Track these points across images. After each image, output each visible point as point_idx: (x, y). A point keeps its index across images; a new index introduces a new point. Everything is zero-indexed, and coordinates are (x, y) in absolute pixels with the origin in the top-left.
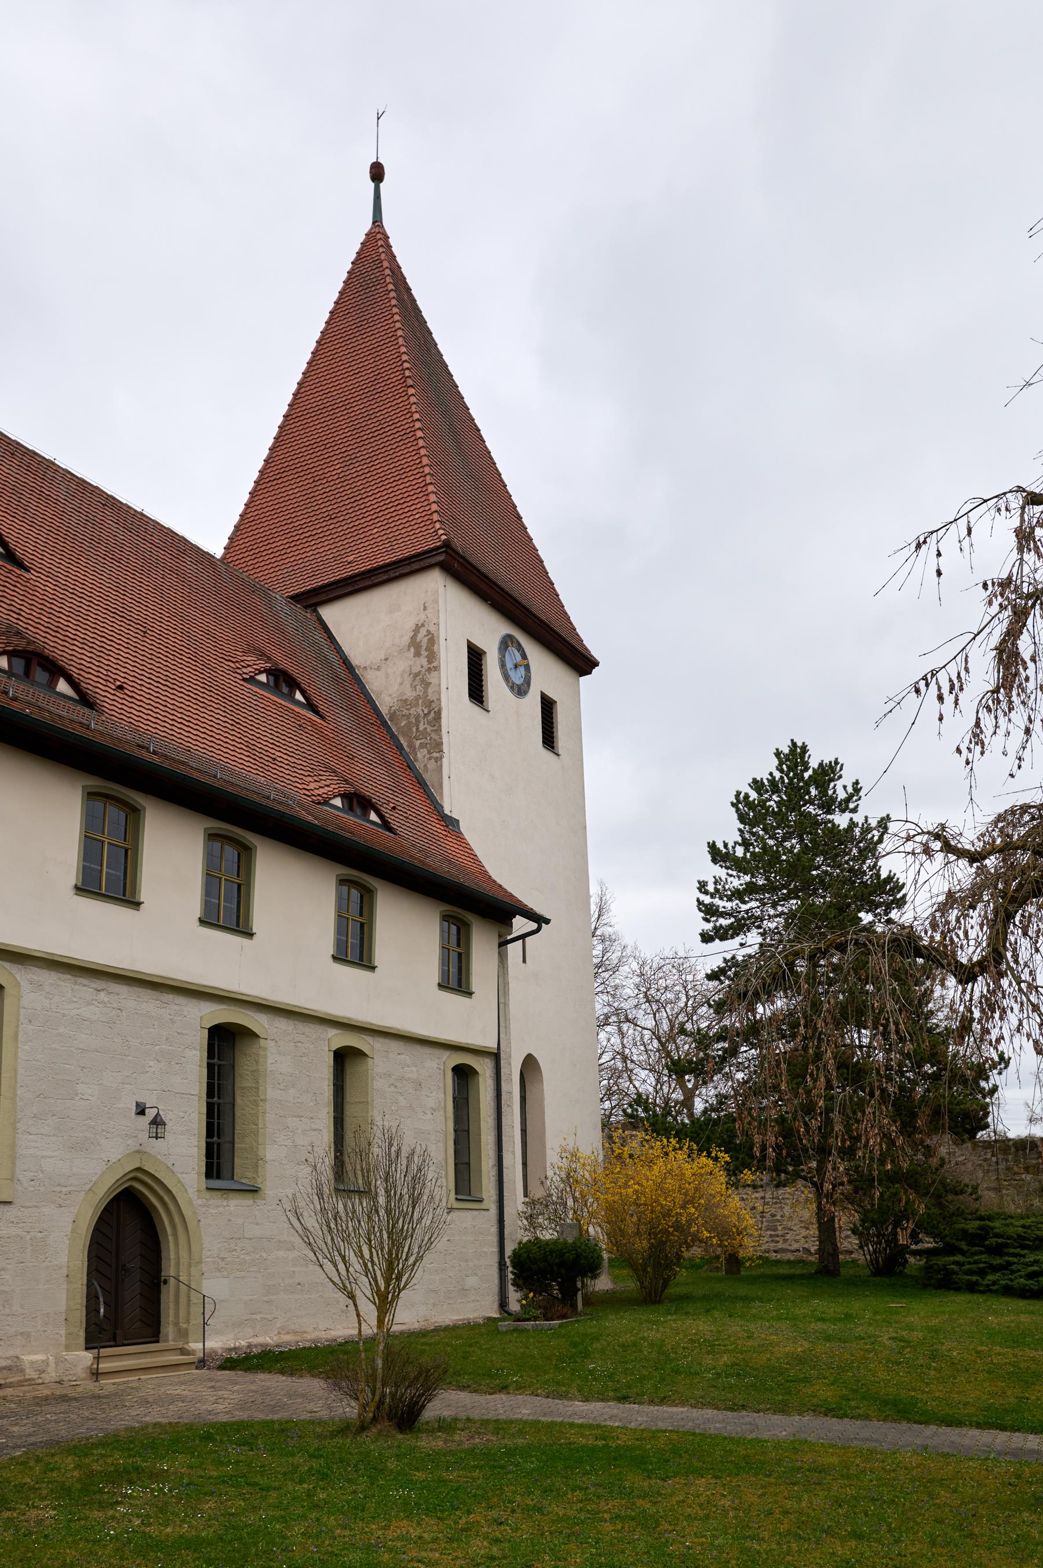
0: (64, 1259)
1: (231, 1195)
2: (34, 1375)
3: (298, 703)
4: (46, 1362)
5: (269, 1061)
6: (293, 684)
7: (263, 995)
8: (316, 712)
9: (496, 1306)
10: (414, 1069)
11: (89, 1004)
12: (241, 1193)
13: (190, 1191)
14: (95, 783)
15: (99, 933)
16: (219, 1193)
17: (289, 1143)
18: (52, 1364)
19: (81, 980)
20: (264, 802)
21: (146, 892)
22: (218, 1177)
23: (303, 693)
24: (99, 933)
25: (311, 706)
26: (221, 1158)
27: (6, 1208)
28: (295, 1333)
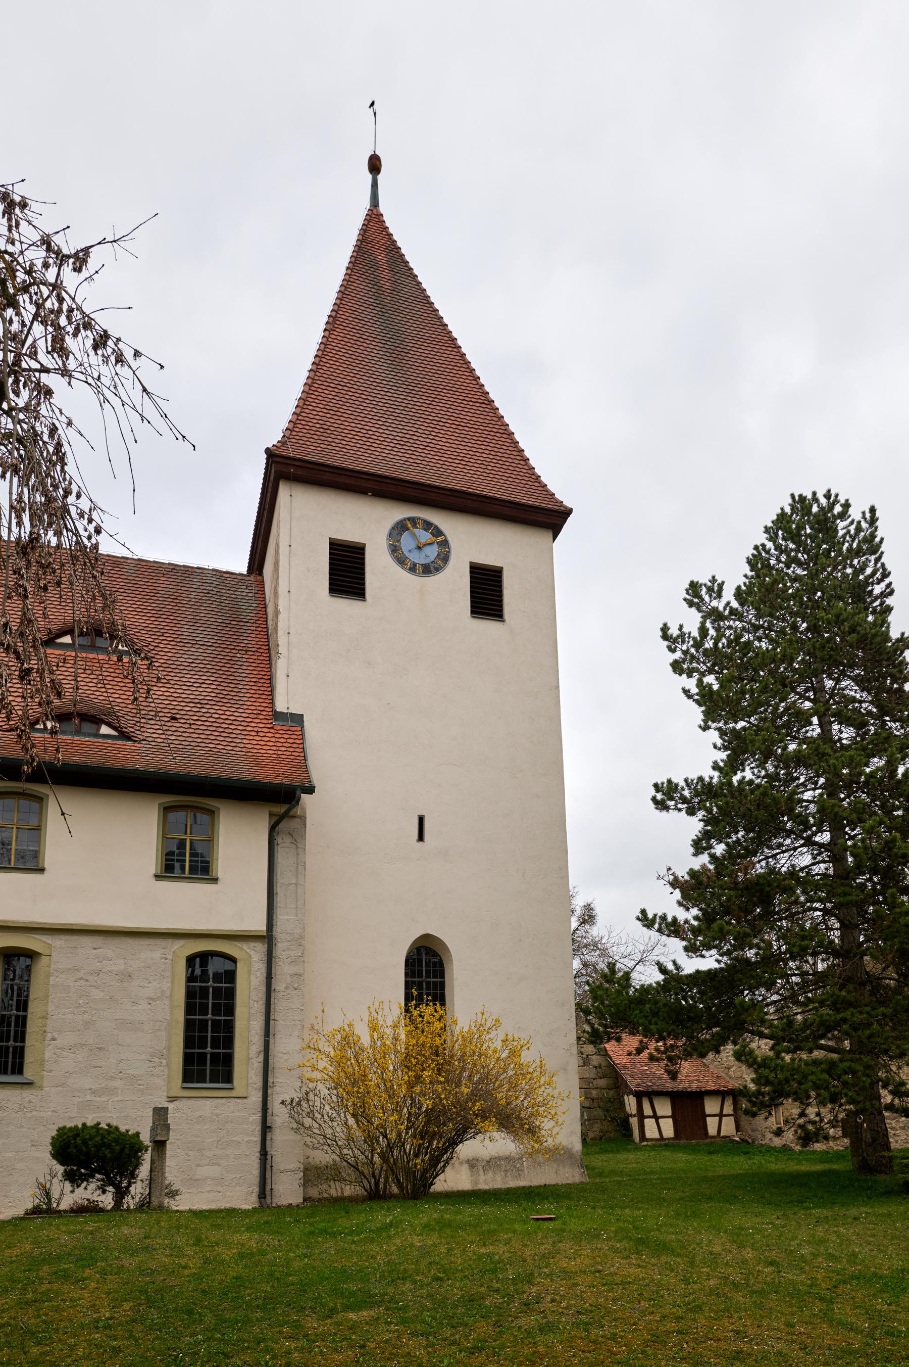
7: (196, 928)
10: (122, 961)
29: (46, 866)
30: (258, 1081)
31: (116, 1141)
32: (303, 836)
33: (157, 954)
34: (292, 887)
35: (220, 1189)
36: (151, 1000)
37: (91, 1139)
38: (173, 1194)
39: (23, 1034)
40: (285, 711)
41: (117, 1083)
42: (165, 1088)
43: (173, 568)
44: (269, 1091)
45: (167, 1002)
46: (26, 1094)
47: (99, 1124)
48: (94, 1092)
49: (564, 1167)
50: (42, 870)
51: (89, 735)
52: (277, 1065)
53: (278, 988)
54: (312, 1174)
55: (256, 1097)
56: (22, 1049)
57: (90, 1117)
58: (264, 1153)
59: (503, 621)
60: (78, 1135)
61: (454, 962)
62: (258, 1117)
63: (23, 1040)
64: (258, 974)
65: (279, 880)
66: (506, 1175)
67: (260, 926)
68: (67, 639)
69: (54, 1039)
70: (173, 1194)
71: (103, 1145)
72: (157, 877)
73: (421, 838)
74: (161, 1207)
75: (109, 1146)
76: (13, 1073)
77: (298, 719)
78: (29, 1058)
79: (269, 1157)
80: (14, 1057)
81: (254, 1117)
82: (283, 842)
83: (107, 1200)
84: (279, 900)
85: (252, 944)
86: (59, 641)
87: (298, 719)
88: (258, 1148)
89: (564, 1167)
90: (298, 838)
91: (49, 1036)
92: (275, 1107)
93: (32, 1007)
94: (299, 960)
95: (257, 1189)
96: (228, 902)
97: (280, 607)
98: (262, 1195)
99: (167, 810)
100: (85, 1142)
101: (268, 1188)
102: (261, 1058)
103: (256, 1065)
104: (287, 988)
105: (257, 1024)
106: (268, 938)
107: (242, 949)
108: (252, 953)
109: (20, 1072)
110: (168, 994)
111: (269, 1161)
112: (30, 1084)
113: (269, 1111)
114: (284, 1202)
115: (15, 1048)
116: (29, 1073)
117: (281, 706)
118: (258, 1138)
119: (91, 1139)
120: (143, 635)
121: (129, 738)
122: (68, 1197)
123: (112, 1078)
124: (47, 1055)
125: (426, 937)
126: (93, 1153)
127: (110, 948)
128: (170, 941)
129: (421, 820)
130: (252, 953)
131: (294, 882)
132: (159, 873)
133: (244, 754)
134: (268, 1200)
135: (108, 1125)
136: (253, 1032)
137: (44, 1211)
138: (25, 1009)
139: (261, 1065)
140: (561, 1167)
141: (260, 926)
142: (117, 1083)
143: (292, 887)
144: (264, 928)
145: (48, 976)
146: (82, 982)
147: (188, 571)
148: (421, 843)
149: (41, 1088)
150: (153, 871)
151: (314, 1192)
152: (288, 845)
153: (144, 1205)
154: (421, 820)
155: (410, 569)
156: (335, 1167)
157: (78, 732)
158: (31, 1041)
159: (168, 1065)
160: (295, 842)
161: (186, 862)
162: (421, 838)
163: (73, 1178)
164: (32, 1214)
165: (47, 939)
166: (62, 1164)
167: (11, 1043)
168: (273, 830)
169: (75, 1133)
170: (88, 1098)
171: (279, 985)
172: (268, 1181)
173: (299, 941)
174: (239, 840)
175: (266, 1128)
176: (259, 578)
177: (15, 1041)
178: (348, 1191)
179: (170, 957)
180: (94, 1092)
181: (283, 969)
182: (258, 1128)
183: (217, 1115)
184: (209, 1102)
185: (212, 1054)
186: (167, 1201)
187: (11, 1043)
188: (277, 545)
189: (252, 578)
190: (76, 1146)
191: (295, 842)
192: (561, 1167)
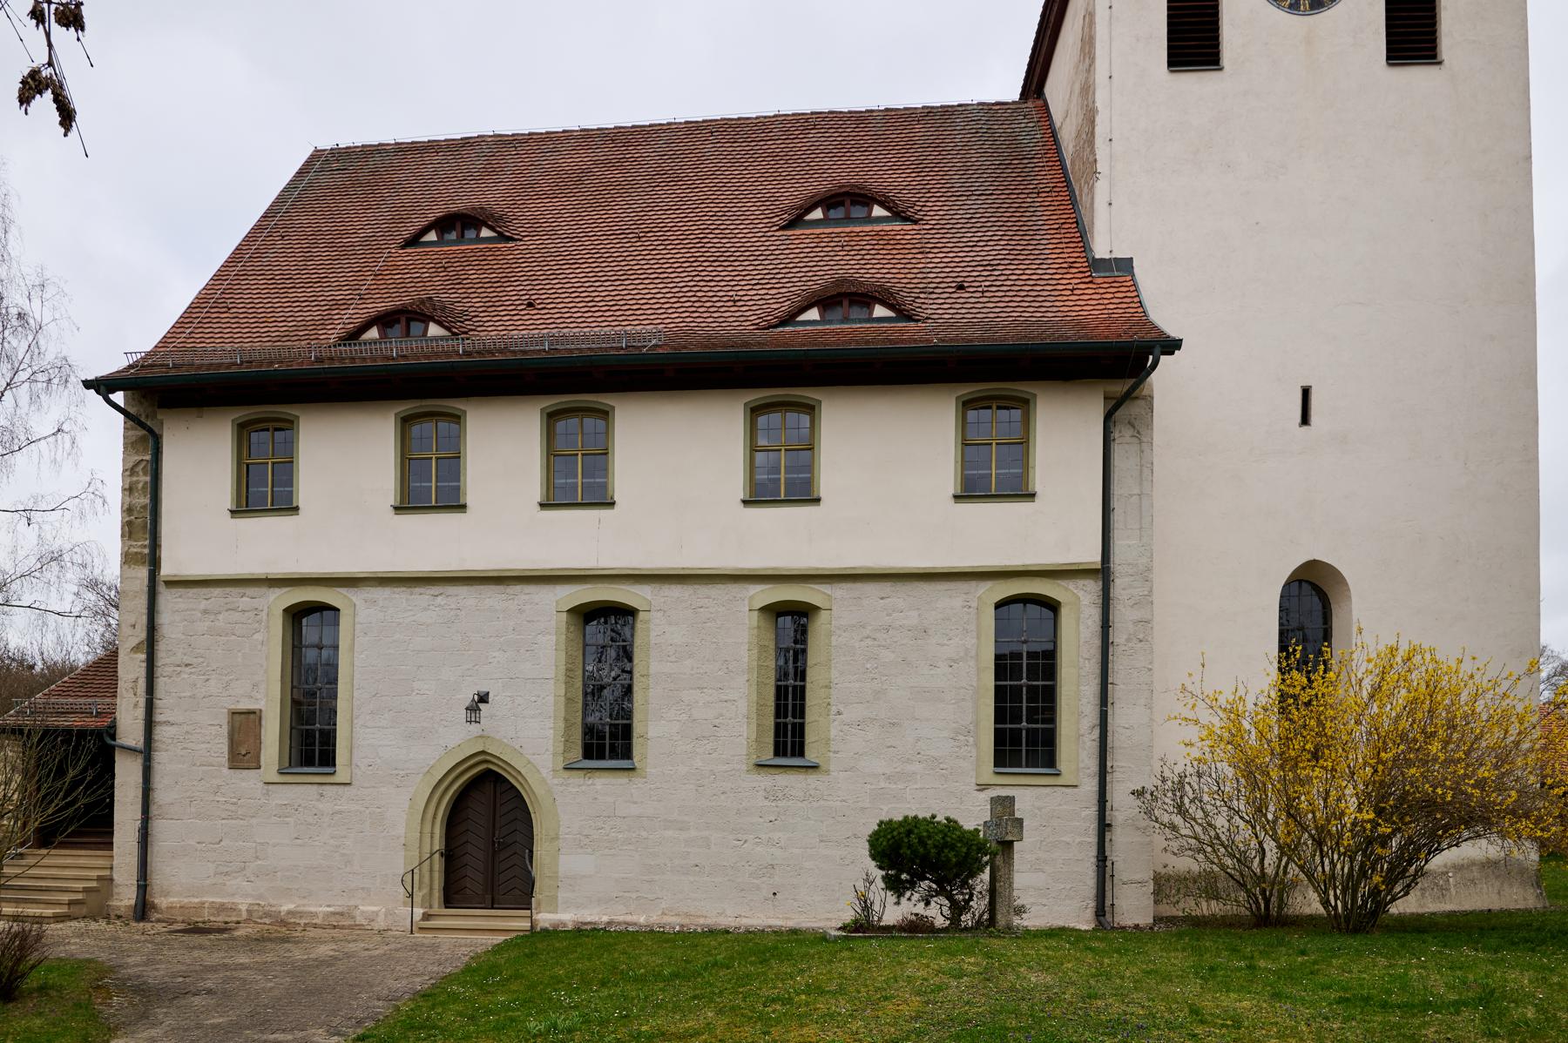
0: (401, 830)
1: (598, 773)
2: (364, 922)
3: (880, 220)
4: (377, 913)
5: (653, 634)
6: (863, 198)
7: (1008, 563)
8: (907, 219)
9: (1089, 913)
10: (915, 614)
11: (425, 609)
12: (772, 771)
13: (544, 772)
14: (967, 390)
15: (431, 542)
16: (581, 773)
17: (684, 717)
18: (382, 916)
19: (417, 590)
20: (233, 370)
21: (471, 497)
22: (785, 755)
23: (882, 205)
24: (431, 542)
25: (899, 215)
26: (606, 739)
27: (347, 788)
28: (687, 915)
29: (822, 495)
30: (1093, 765)
31: (960, 839)
32: (1149, 425)
33: (958, 602)
34: (1135, 499)
35: (1045, 901)
36: (952, 662)
37: (929, 837)
38: (1020, 911)
39: (803, 707)
40: (1107, 256)
41: (916, 767)
42: (973, 773)
43: (929, 112)
44: (1108, 778)
45: (972, 663)
46: (811, 779)
47: (934, 817)
48: (889, 778)
49: (1511, 886)
50: (817, 501)
51: (860, 321)
52: (1117, 744)
53: (1116, 641)
54: (1163, 885)
55: (1090, 786)
56: (802, 726)
57: (885, 808)
58: (1102, 859)
59: (1440, 63)
60: (909, 832)
61: (1354, 599)
62: (1092, 811)
63: (802, 715)
64: (1090, 622)
65: (1117, 490)
66: (1423, 895)
67: (1093, 557)
68: (817, 214)
69: (839, 713)
70: (1020, 911)
71: (945, 845)
72: (957, 498)
73: (1305, 420)
74: (1009, 928)
75: (952, 847)
76: (793, 755)
77: (1126, 265)
78: (810, 737)
79: (1109, 863)
80: (793, 736)
81: (1088, 812)
82: (1122, 436)
83: (937, 913)
84: (1117, 518)
85: (1081, 582)
86: (808, 217)
87: (1126, 265)
88: (1093, 852)
89: (1511, 886)
90: (1141, 428)
91: (834, 709)
92: (1120, 795)
93: (811, 675)
94: (1147, 600)
95: (1092, 904)
96: (1049, 526)
97: (1100, 103)
98: (1100, 911)
99: (966, 405)
100: (921, 841)
101: (1108, 903)
102: (1096, 733)
103: (1089, 744)
104: (1128, 640)
105: (1091, 689)
106: (1103, 573)
107: (1067, 589)
108: (1081, 594)
109: (802, 754)
110: (973, 653)
111: (1108, 870)
112: (815, 767)
113: (1108, 805)
114: (1128, 921)
115: (794, 725)
116: (811, 754)
117: (1101, 251)
118: (1093, 839)
119: (929, 837)
120: (906, 195)
121: (910, 318)
122: (893, 911)
123: (909, 761)
124: (833, 733)
125: (1312, 565)
126: (911, 852)
127: (900, 595)
128: (973, 583)
129: (1306, 393)
130: (1081, 594)
131: (1137, 491)
132: (959, 493)
133: (1070, 310)
134: (1108, 917)
135: (947, 819)
136: (1084, 701)
137: (863, 927)
138: (803, 678)
139: (1097, 744)
140: (1506, 886)
141: (1090, 555)
142: (916, 767)
143: (1135, 499)
144: (1099, 558)
145: (830, 634)
146: (869, 642)
147: (947, 112)
148: (1305, 428)
149: (827, 772)
150: (951, 491)
151: (1168, 910)
152: (1128, 439)
153: (989, 924)
154: (1306, 393)
155: (1291, 6)
156: (1209, 877)
157: (846, 320)
158: (811, 715)
159: (976, 744)
160: (1138, 435)
161: (994, 477)
162: (1305, 420)
163: (896, 886)
164: (856, 930)
165: (826, 588)
166: (881, 868)
167: (790, 718)
168: (1108, 418)
169: (911, 826)
170: (882, 785)
171: (1118, 636)
172: (1108, 894)
173: (1145, 575)
174: (1064, 432)
175: (1104, 827)
176: (1040, 102)
177: (794, 717)
178: (1229, 909)
179: (974, 604)
180: (889, 778)
181: (1123, 615)
182: (1093, 826)
183: (1039, 809)
184: (1029, 791)
185: (1028, 730)
186: (1016, 921)
187: (790, 718)
188: (1090, 17)
189: (1030, 104)
190: (910, 846)
191: (1138, 435)
192: (1506, 886)
